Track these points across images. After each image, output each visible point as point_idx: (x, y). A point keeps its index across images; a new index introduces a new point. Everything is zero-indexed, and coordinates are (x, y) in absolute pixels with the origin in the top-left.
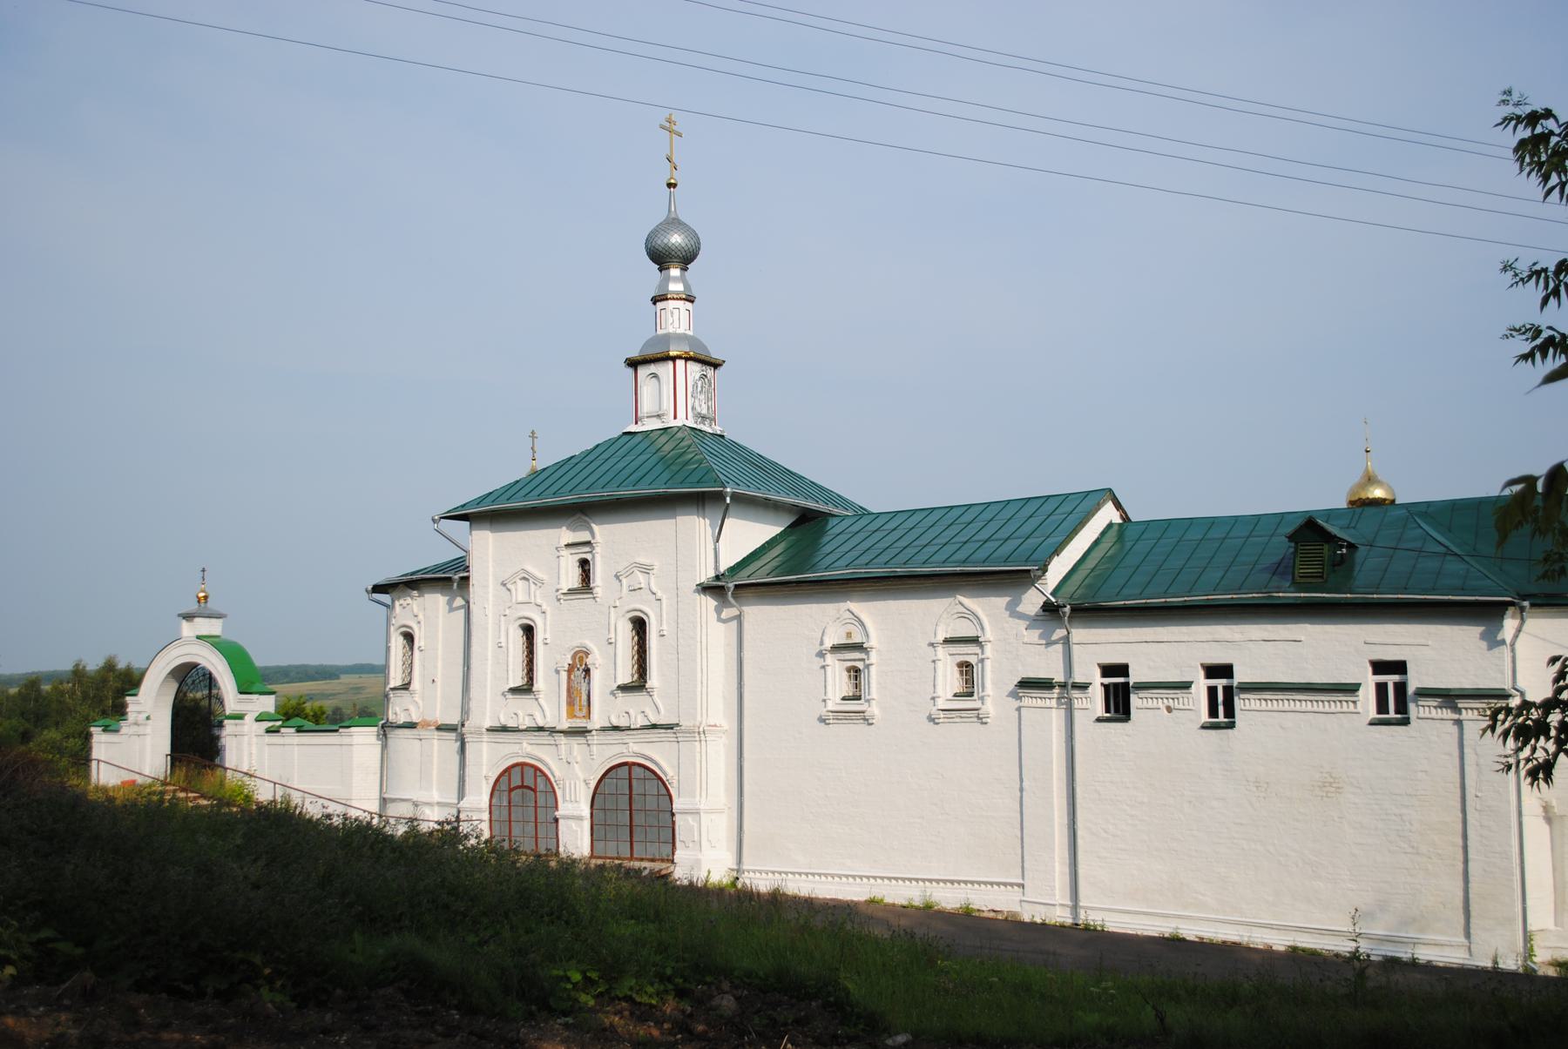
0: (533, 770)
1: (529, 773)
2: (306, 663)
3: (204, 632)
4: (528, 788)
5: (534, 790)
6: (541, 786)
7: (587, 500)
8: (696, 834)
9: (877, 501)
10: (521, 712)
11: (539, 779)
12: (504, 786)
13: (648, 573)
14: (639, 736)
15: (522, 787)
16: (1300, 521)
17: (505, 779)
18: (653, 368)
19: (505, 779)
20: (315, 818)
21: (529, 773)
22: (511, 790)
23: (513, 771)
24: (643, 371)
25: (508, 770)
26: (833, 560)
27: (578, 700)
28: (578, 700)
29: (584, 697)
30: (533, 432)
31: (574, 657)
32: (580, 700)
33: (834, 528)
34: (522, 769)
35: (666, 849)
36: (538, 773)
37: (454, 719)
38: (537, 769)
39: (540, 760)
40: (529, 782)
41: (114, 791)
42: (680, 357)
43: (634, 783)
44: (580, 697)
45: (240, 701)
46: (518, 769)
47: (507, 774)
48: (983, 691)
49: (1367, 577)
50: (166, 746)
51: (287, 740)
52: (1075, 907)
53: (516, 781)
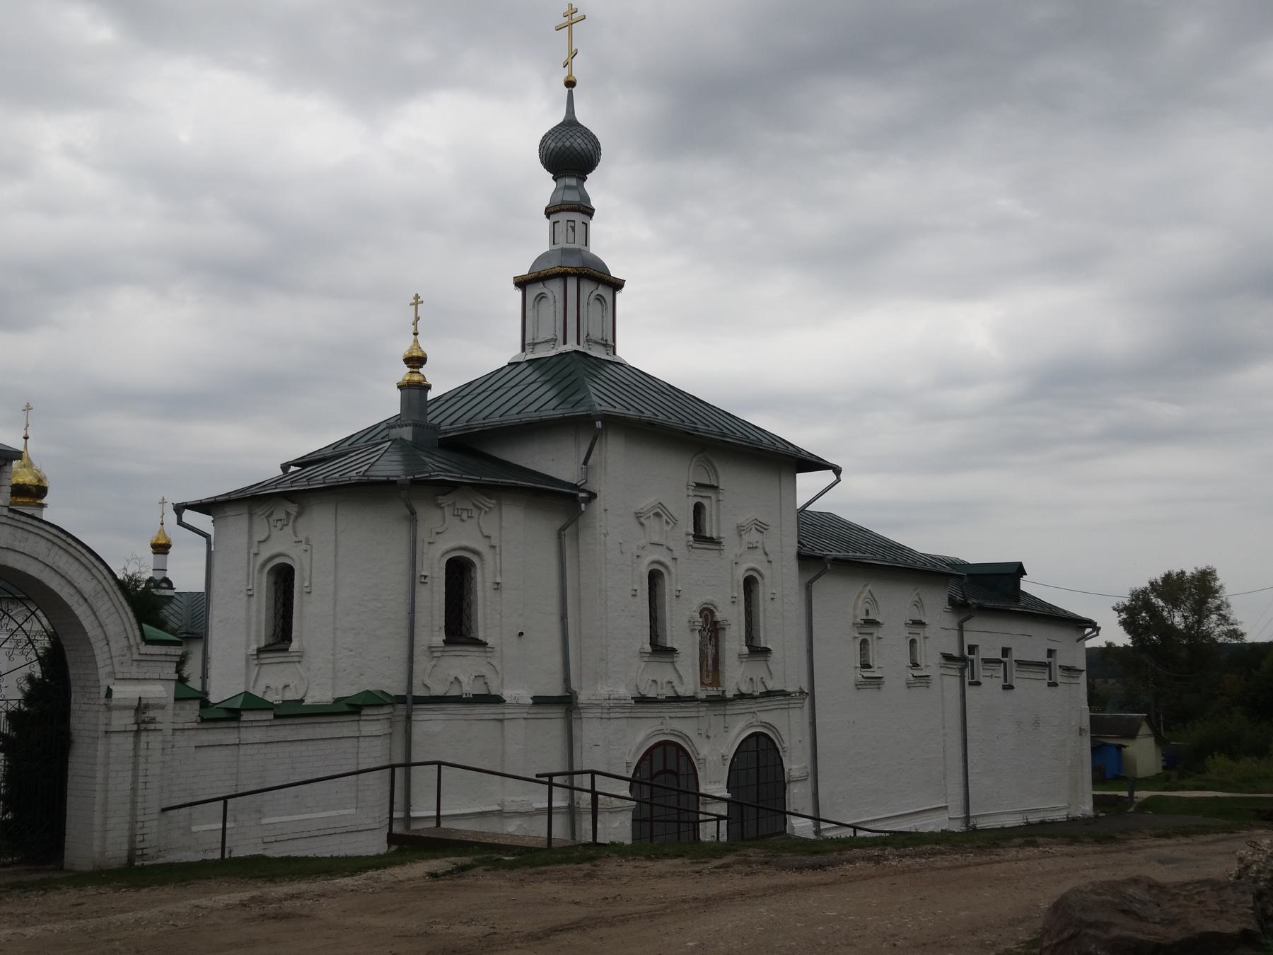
4: (670, 771)
6: (683, 769)
7: (488, 483)
10: (658, 679)
11: (681, 761)
13: (762, 532)
14: (766, 704)
19: (645, 765)
25: (649, 752)
27: (711, 667)
28: (711, 667)
30: (417, 297)
32: (707, 665)
34: (758, 738)
36: (681, 753)
37: (556, 690)
40: (671, 765)
41: (1219, 608)
44: (707, 661)
46: (660, 750)
47: (648, 757)
48: (671, 717)
50: (1091, 805)
53: (658, 766)
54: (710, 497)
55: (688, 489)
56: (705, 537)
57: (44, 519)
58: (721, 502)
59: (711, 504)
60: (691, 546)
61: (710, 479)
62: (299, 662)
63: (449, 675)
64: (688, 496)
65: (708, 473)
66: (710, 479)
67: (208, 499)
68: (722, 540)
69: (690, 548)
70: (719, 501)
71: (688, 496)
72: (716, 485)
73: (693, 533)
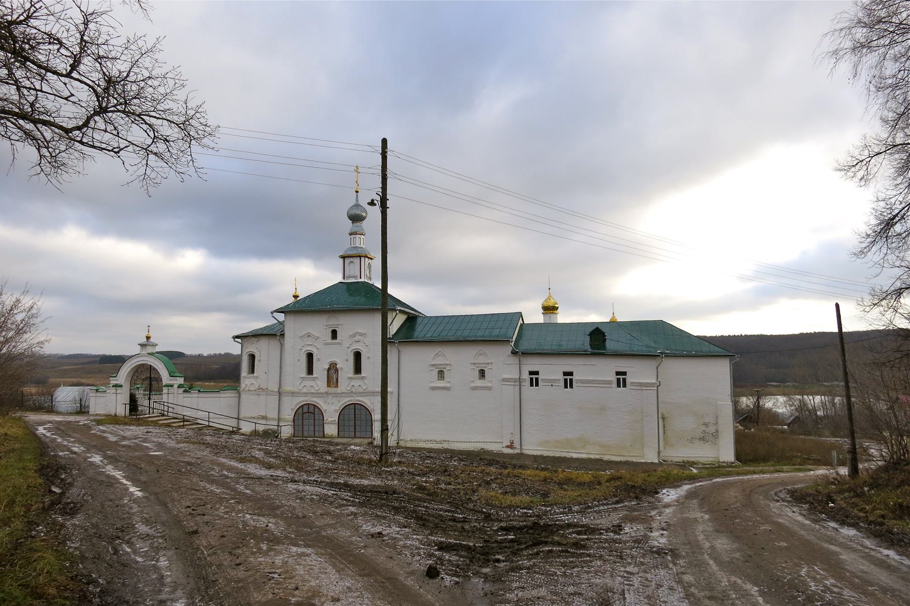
0: (313, 406)
1: (311, 408)
2: (122, 354)
3: (150, 352)
5: (314, 414)
8: (377, 427)
9: (428, 314)
12: (300, 411)
15: (308, 412)
16: (591, 329)
17: (301, 409)
18: (351, 259)
20: (29, 342)
21: (311, 408)
22: (303, 414)
23: (304, 407)
24: (347, 261)
26: (420, 331)
29: (335, 380)
31: (330, 365)
33: (419, 320)
35: (369, 434)
38: (315, 406)
39: (317, 403)
42: (363, 256)
43: (356, 410)
45: (170, 380)
49: (610, 345)
51: (194, 395)
52: (521, 449)
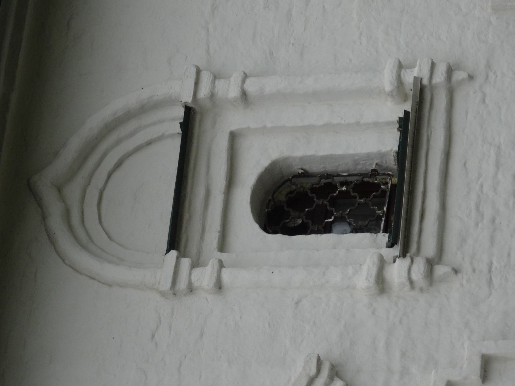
54: (233, 137)
55: (191, 289)
56: (401, 155)
57: (396, 148)
58: (251, 86)
59: (264, 130)
60: (431, 264)
61: (160, 138)
62: (216, 77)
63: (94, 131)
64: (219, 286)
65: (138, 149)
66: (160, 138)
67: (428, 140)
68: (409, 78)
69: (440, 270)
70: (244, 94)
71: (219, 286)
72: (181, 112)
73: (365, 198)
